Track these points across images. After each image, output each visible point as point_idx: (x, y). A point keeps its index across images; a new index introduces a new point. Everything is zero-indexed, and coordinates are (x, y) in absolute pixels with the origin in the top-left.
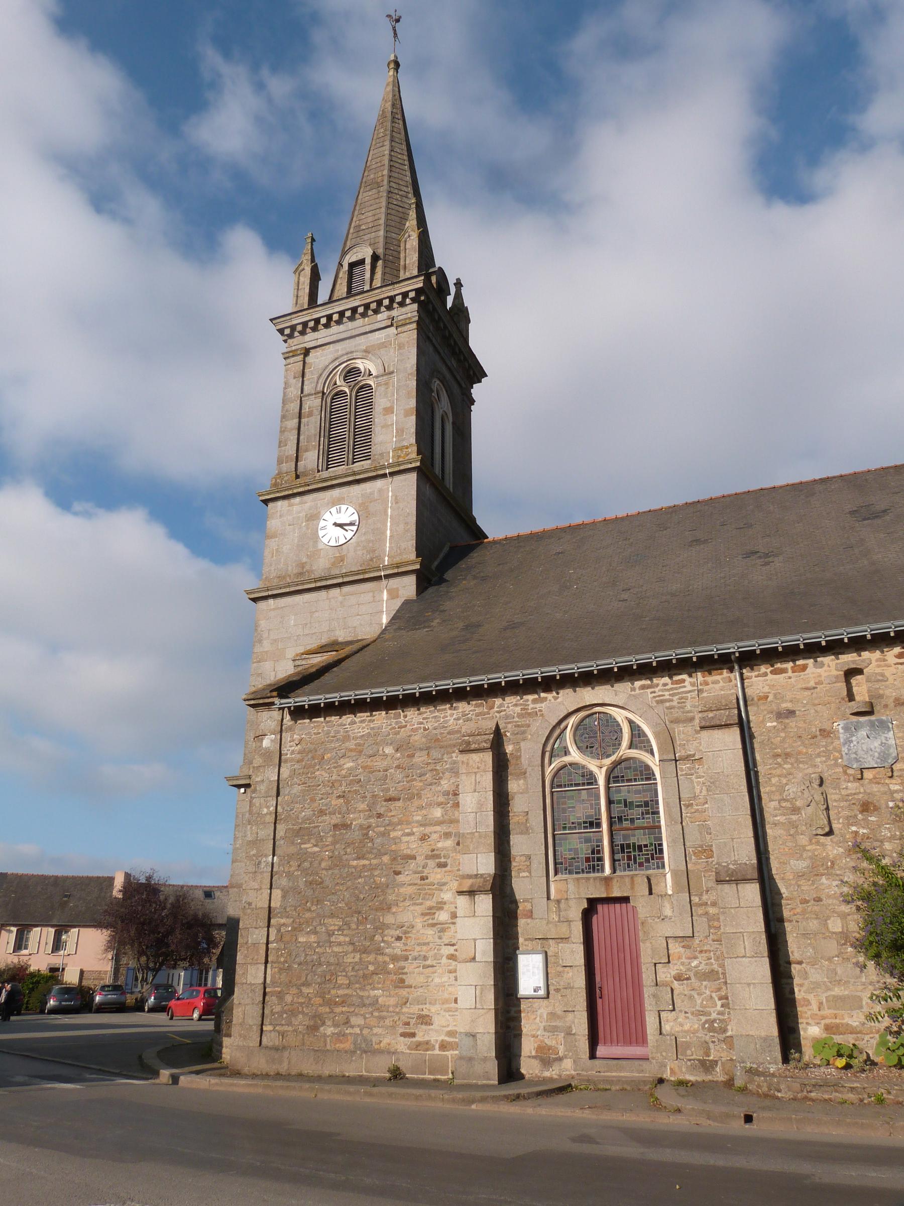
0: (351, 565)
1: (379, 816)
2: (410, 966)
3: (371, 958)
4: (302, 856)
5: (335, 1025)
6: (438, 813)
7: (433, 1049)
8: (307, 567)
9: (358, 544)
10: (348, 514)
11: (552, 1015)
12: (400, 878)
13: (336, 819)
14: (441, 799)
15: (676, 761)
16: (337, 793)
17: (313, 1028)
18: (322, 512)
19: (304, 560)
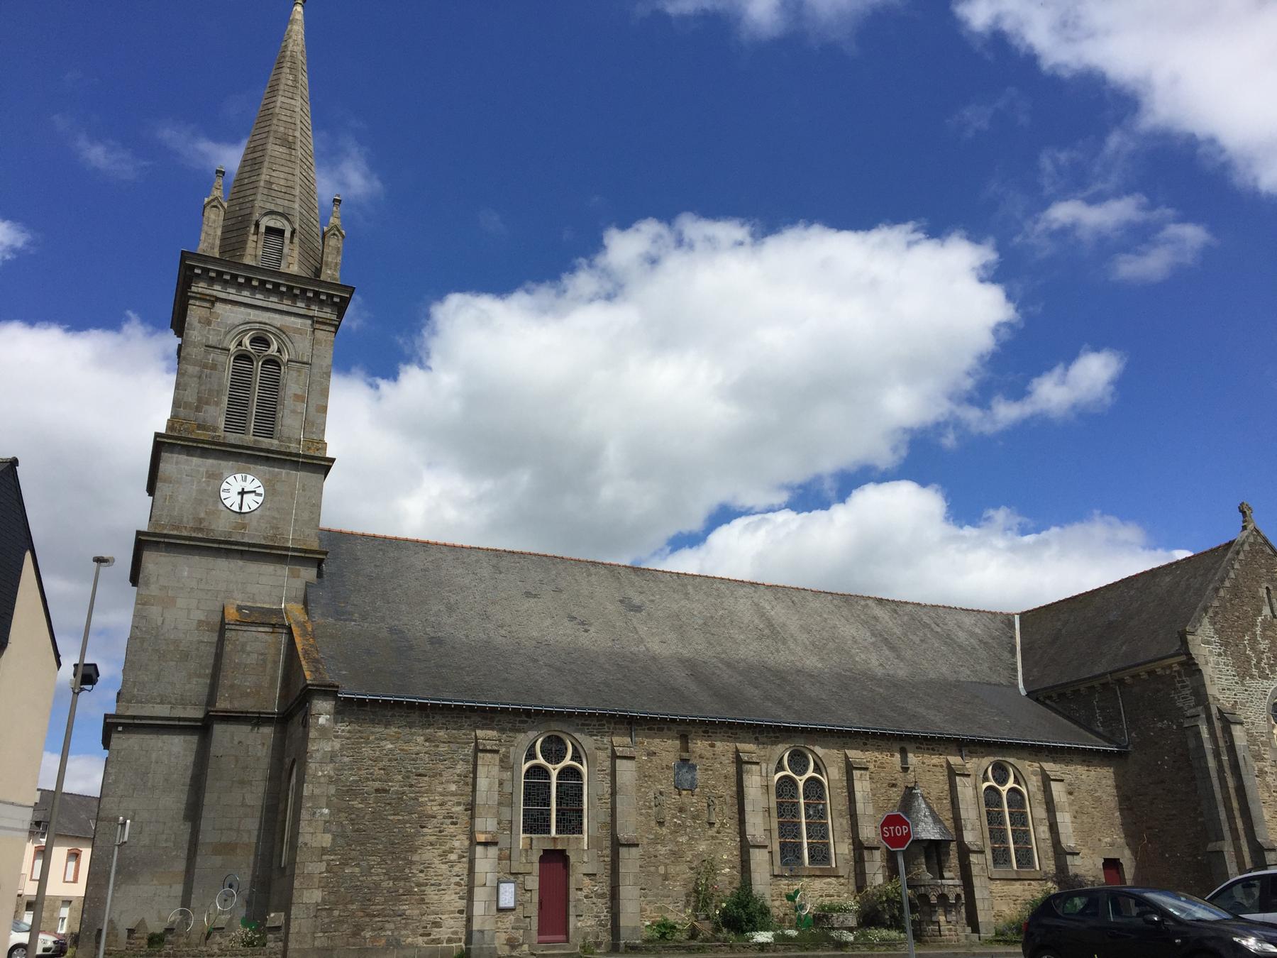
0: (255, 534)
1: (411, 786)
2: (429, 890)
3: (402, 884)
4: (351, 810)
5: (373, 930)
6: (453, 788)
7: (793, 783)
8: (205, 524)
9: (262, 517)
10: (252, 483)
11: (517, 920)
12: (425, 830)
13: (377, 785)
14: (456, 778)
15: (202, 728)
16: (381, 765)
17: (355, 934)
18: (225, 475)
19: (202, 515)
